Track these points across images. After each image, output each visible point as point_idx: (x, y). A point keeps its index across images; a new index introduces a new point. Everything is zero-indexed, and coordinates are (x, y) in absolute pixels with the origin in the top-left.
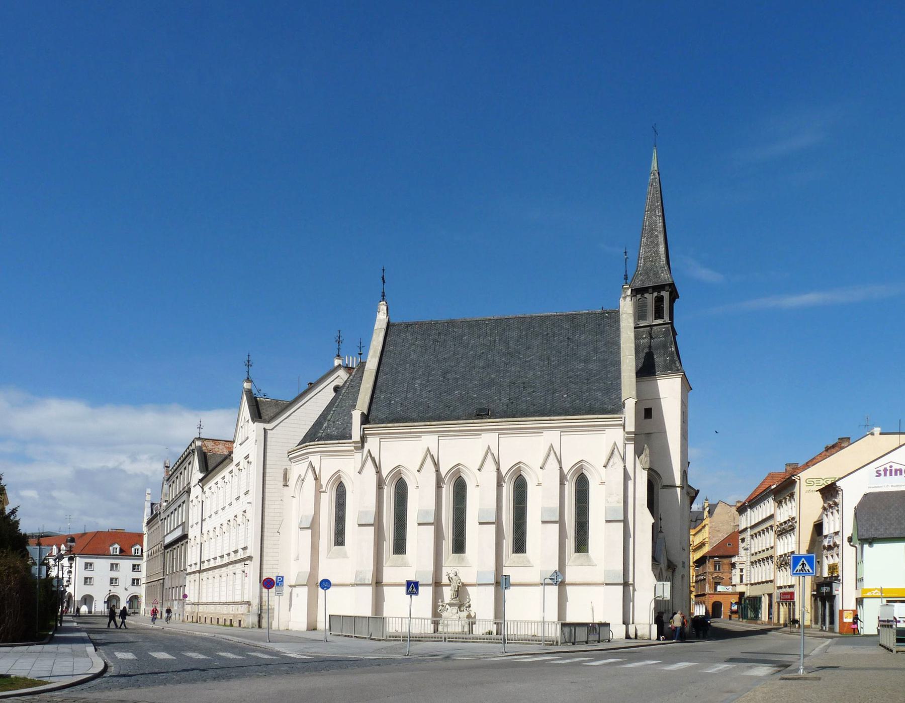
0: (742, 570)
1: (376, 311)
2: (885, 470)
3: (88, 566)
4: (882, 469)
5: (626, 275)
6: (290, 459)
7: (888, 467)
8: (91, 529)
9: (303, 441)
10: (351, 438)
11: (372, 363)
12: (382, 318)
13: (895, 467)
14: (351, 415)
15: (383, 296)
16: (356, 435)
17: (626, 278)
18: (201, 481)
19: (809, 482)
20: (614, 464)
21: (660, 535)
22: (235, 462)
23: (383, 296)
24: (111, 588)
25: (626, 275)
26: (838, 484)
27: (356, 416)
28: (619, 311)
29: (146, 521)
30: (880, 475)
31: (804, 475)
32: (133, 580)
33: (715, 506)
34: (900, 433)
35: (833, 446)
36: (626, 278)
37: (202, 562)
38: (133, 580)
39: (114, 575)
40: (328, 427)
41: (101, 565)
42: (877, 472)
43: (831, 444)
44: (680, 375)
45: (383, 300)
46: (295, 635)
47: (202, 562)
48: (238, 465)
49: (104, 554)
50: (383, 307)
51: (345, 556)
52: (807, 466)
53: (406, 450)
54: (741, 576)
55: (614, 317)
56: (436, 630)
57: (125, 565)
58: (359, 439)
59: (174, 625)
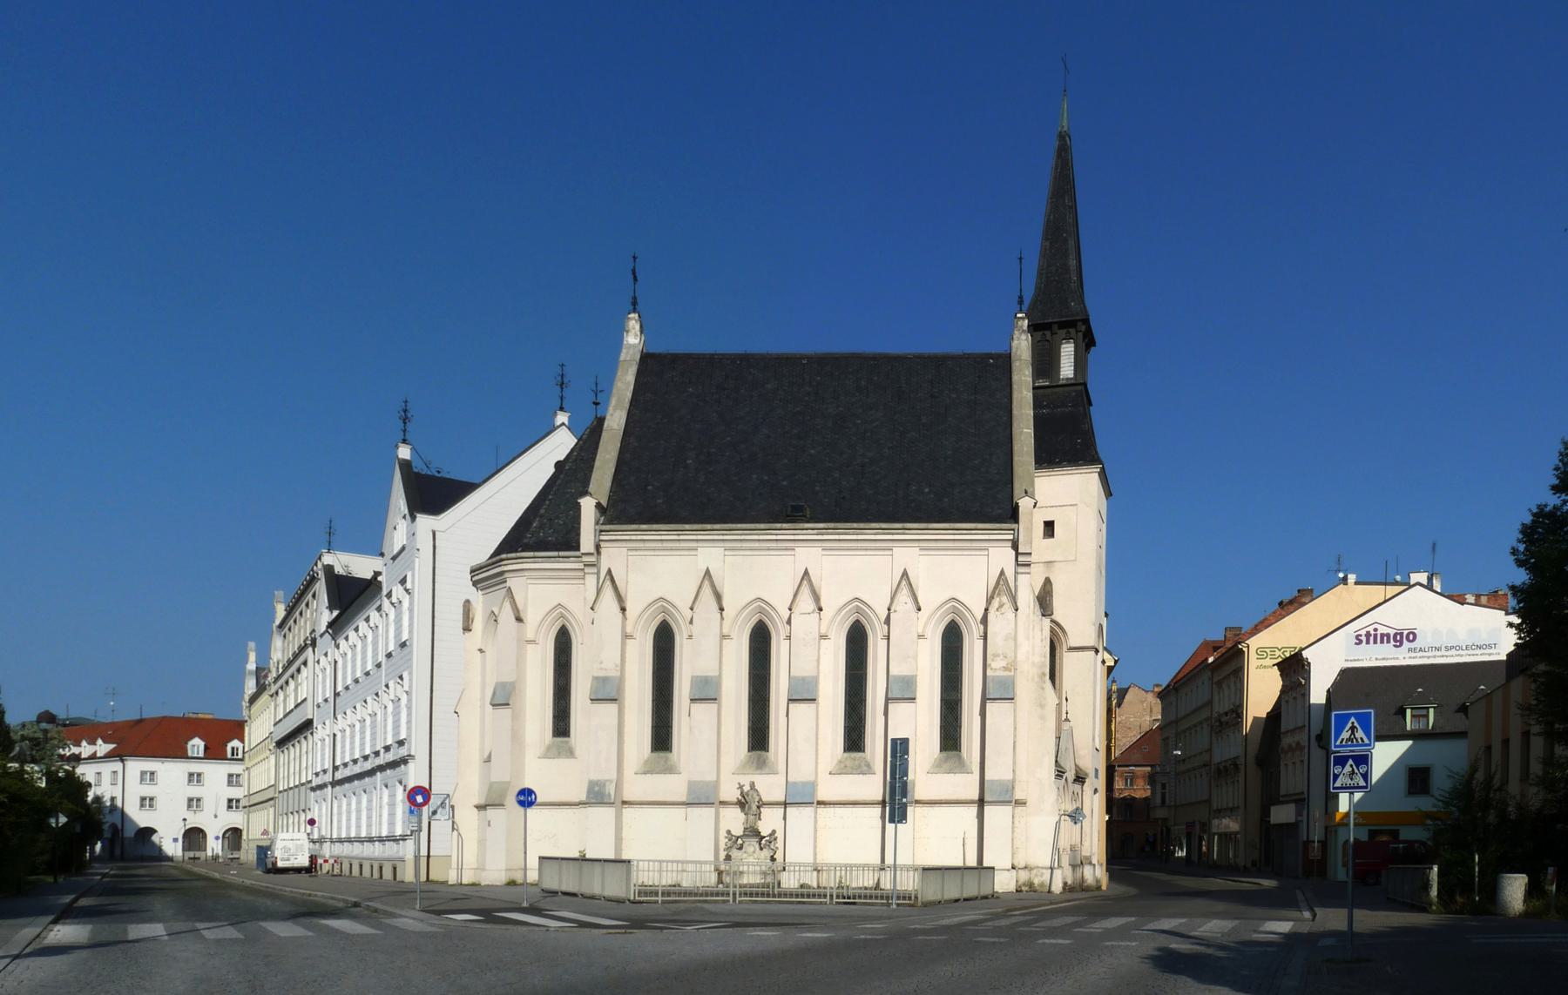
0: (1164, 786)
1: (622, 330)
2: (1368, 635)
3: (149, 777)
4: (1363, 632)
5: (1021, 297)
6: (475, 584)
7: (1371, 629)
8: (151, 712)
9: (498, 552)
10: (578, 549)
11: (616, 420)
12: (633, 339)
13: (1382, 630)
14: (579, 506)
15: (635, 303)
16: (587, 540)
17: (1021, 302)
18: (331, 625)
19: (1261, 652)
20: (1001, 606)
21: (1066, 726)
22: (385, 592)
23: (635, 303)
24: (190, 816)
25: (1021, 297)
26: (1305, 654)
27: (588, 506)
28: (1009, 356)
29: (247, 698)
30: (1360, 642)
31: (1254, 643)
32: (190, 800)
33: (1126, 690)
34: (1385, 584)
35: (1291, 602)
36: (1021, 302)
37: (335, 768)
38: (190, 800)
39: (194, 791)
40: (541, 526)
41: (170, 772)
42: (1357, 637)
43: (1286, 598)
44: (1096, 469)
45: (634, 311)
46: (485, 895)
47: (335, 768)
48: (389, 595)
49: (177, 752)
50: (633, 324)
51: (570, 753)
52: (1256, 630)
53: (663, 569)
54: (1163, 796)
55: (1004, 362)
56: (720, 881)
57: (215, 772)
58: (592, 549)
59: (1095, 850)
